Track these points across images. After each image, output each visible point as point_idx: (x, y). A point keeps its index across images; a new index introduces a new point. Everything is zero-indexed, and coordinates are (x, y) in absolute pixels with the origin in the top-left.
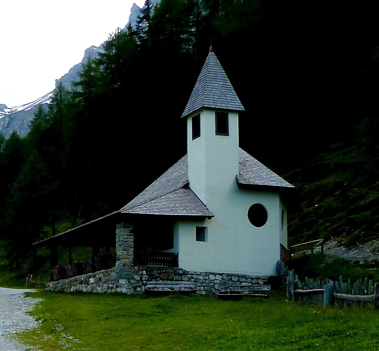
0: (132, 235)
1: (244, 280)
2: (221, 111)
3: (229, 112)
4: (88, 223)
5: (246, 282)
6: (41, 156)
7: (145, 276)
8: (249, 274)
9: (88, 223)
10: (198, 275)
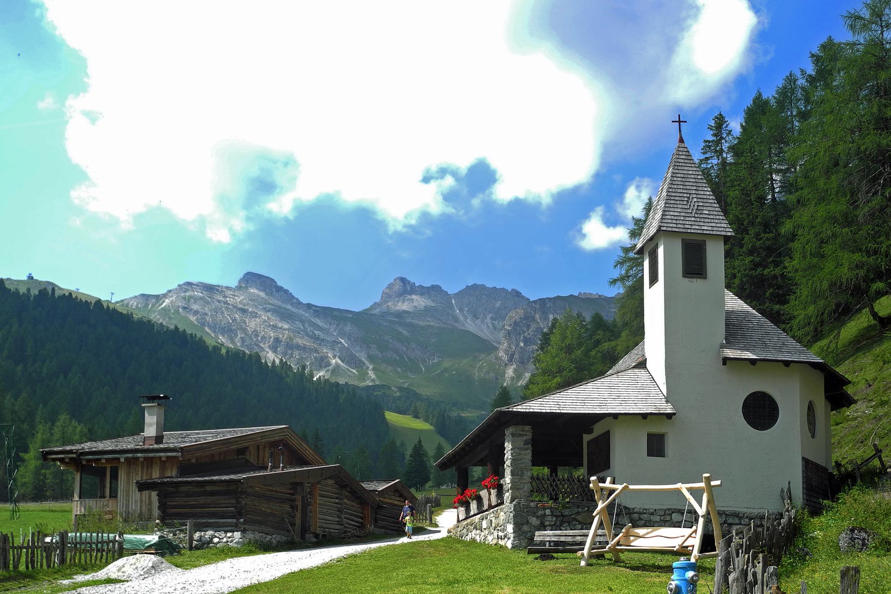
0: (527, 449)
1: (737, 521)
2: (170, 454)
3: (581, 223)
4: (199, 479)
5: (740, 524)
6: (315, 379)
7: (549, 518)
8: (745, 510)
9: (199, 479)
10: (652, 514)
